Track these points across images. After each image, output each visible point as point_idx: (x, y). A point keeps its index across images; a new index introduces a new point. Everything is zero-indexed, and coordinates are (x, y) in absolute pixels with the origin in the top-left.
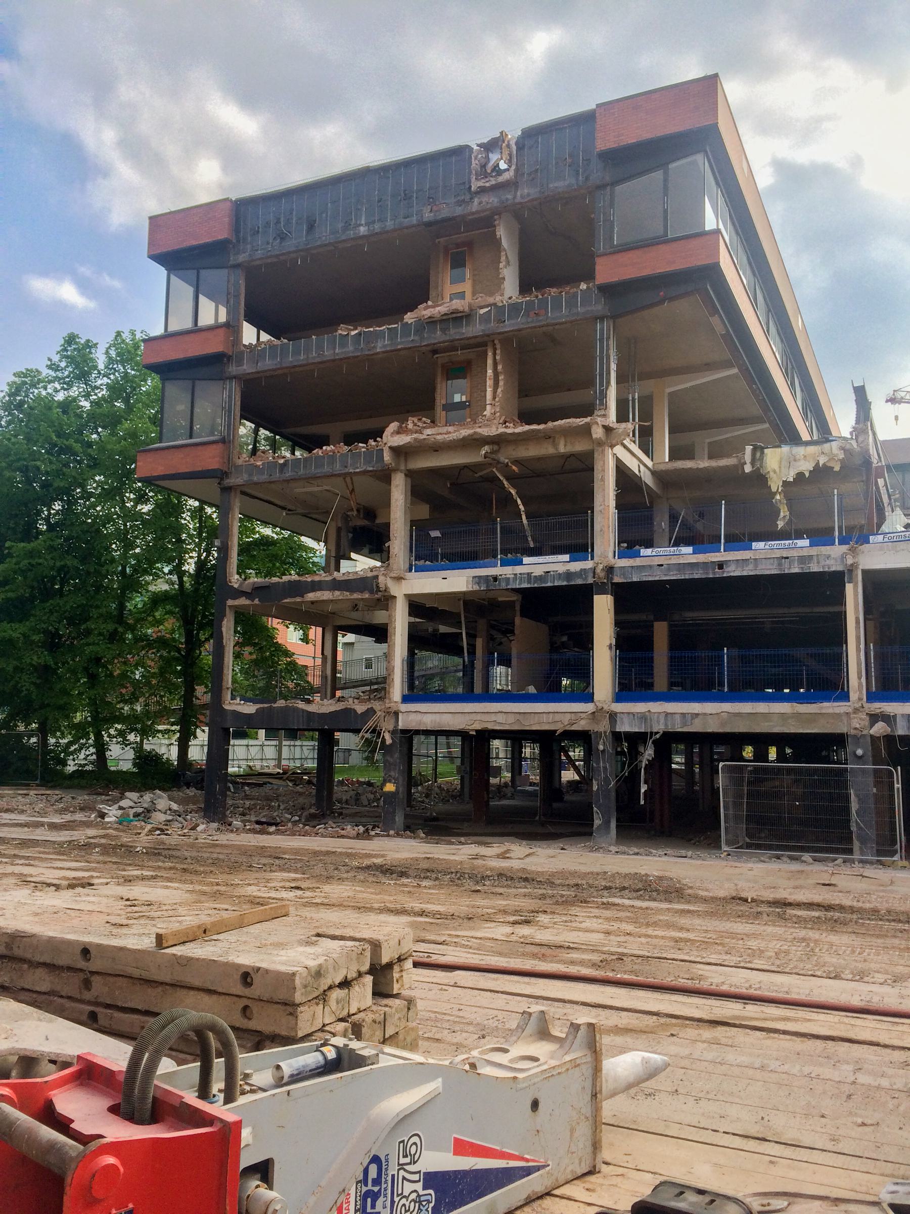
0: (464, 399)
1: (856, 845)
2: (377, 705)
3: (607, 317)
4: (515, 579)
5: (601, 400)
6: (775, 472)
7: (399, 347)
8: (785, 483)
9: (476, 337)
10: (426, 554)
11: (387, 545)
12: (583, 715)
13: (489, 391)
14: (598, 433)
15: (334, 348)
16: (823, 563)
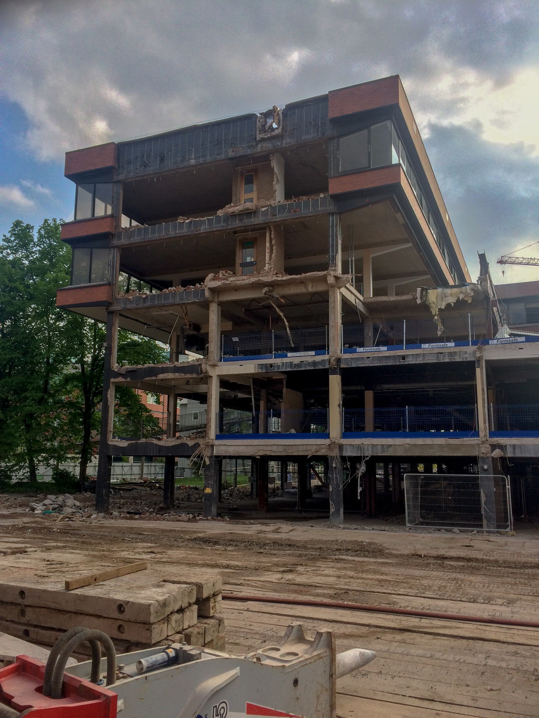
0: (253, 260)
1: (485, 522)
2: (201, 441)
4: (283, 365)
5: (333, 261)
6: (434, 303)
8: (440, 310)
9: (260, 224)
12: (323, 446)
13: (267, 255)
14: (331, 280)
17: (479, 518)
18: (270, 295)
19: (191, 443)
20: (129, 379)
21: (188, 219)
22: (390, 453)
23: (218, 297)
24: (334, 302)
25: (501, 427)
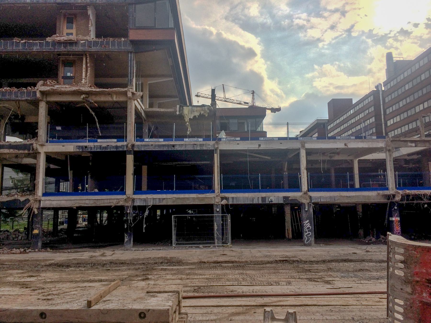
0: (72, 75)
1: (216, 240)
2: (31, 198)
3: (133, 52)
4: (94, 148)
5: (131, 83)
6: (187, 115)
7: (44, 50)
8: (190, 119)
9: (79, 51)
10: (53, 136)
11: (36, 131)
12: (122, 200)
13: (84, 74)
14: (130, 95)
15: (13, 47)
16: (207, 147)
17: (213, 239)
18: (86, 100)
19: (22, 199)
21: (22, 40)
22: (164, 203)
23: (46, 99)
24: (131, 109)
25: (226, 187)
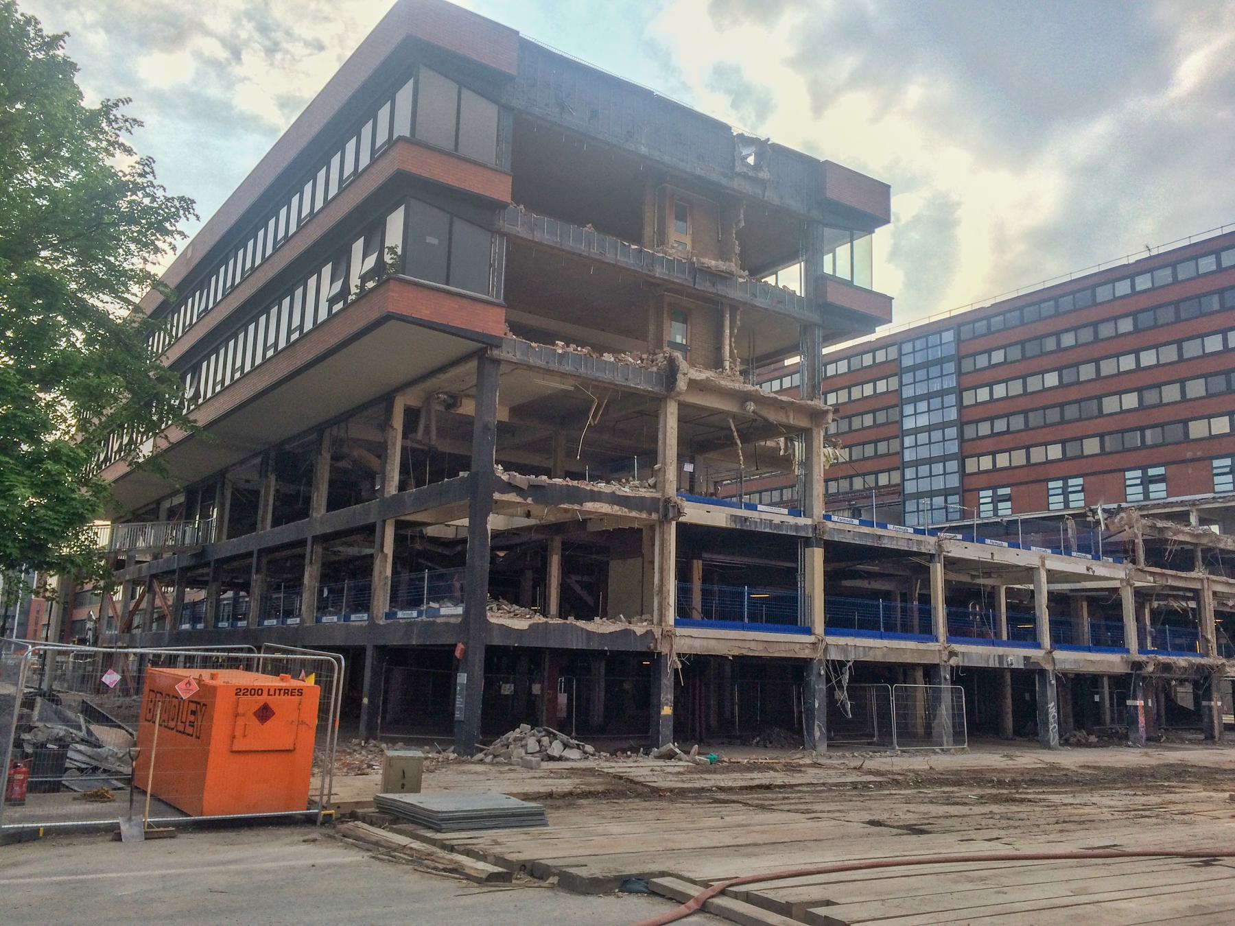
20: (529, 500)
25: (835, 623)
